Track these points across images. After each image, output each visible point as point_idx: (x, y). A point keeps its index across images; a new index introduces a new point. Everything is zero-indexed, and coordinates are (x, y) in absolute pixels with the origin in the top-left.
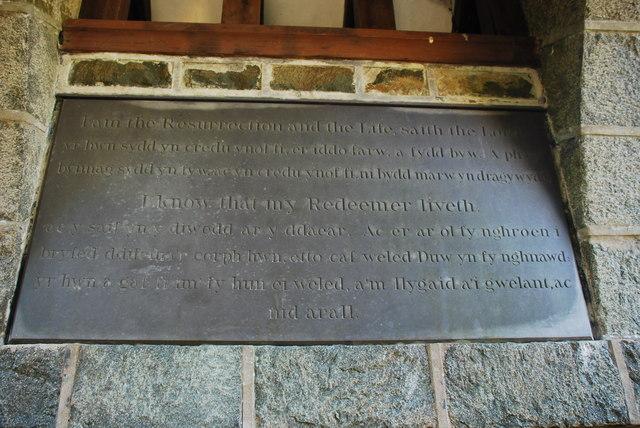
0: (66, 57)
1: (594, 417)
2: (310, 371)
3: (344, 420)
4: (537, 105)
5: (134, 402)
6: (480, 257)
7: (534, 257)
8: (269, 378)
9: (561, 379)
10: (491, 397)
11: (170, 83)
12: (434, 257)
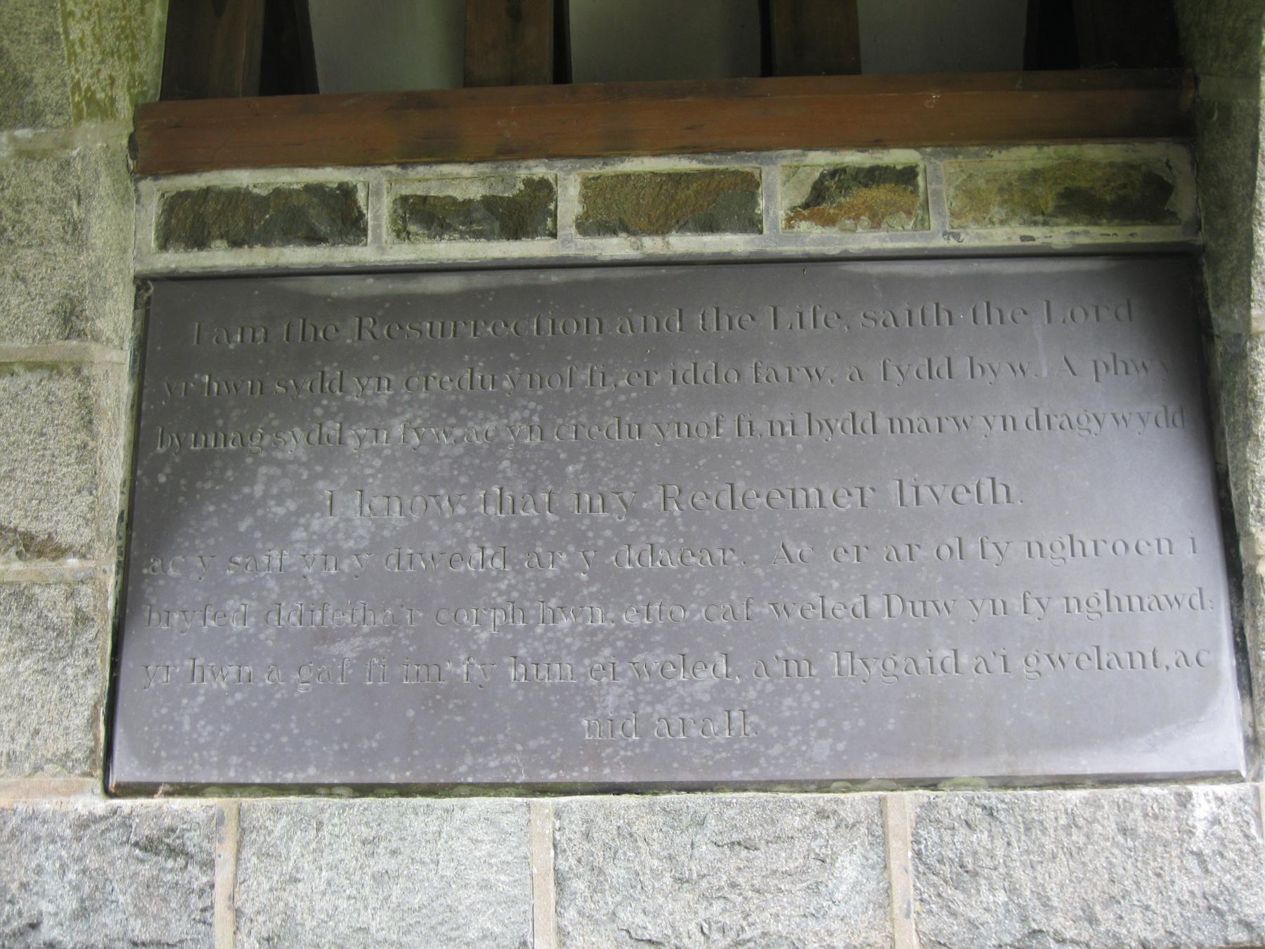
0: (147, 185)
1: (1207, 932)
2: (656, 847)
3: (716, 936)
4: (1182, 238)
5: (343, 904)
6: (1016, 604)
7: (1136, 601)
8: (579, 861)
9: (1145, 863)
10: (1002, 897)
11: (364, 232)
12: (919, 607)
